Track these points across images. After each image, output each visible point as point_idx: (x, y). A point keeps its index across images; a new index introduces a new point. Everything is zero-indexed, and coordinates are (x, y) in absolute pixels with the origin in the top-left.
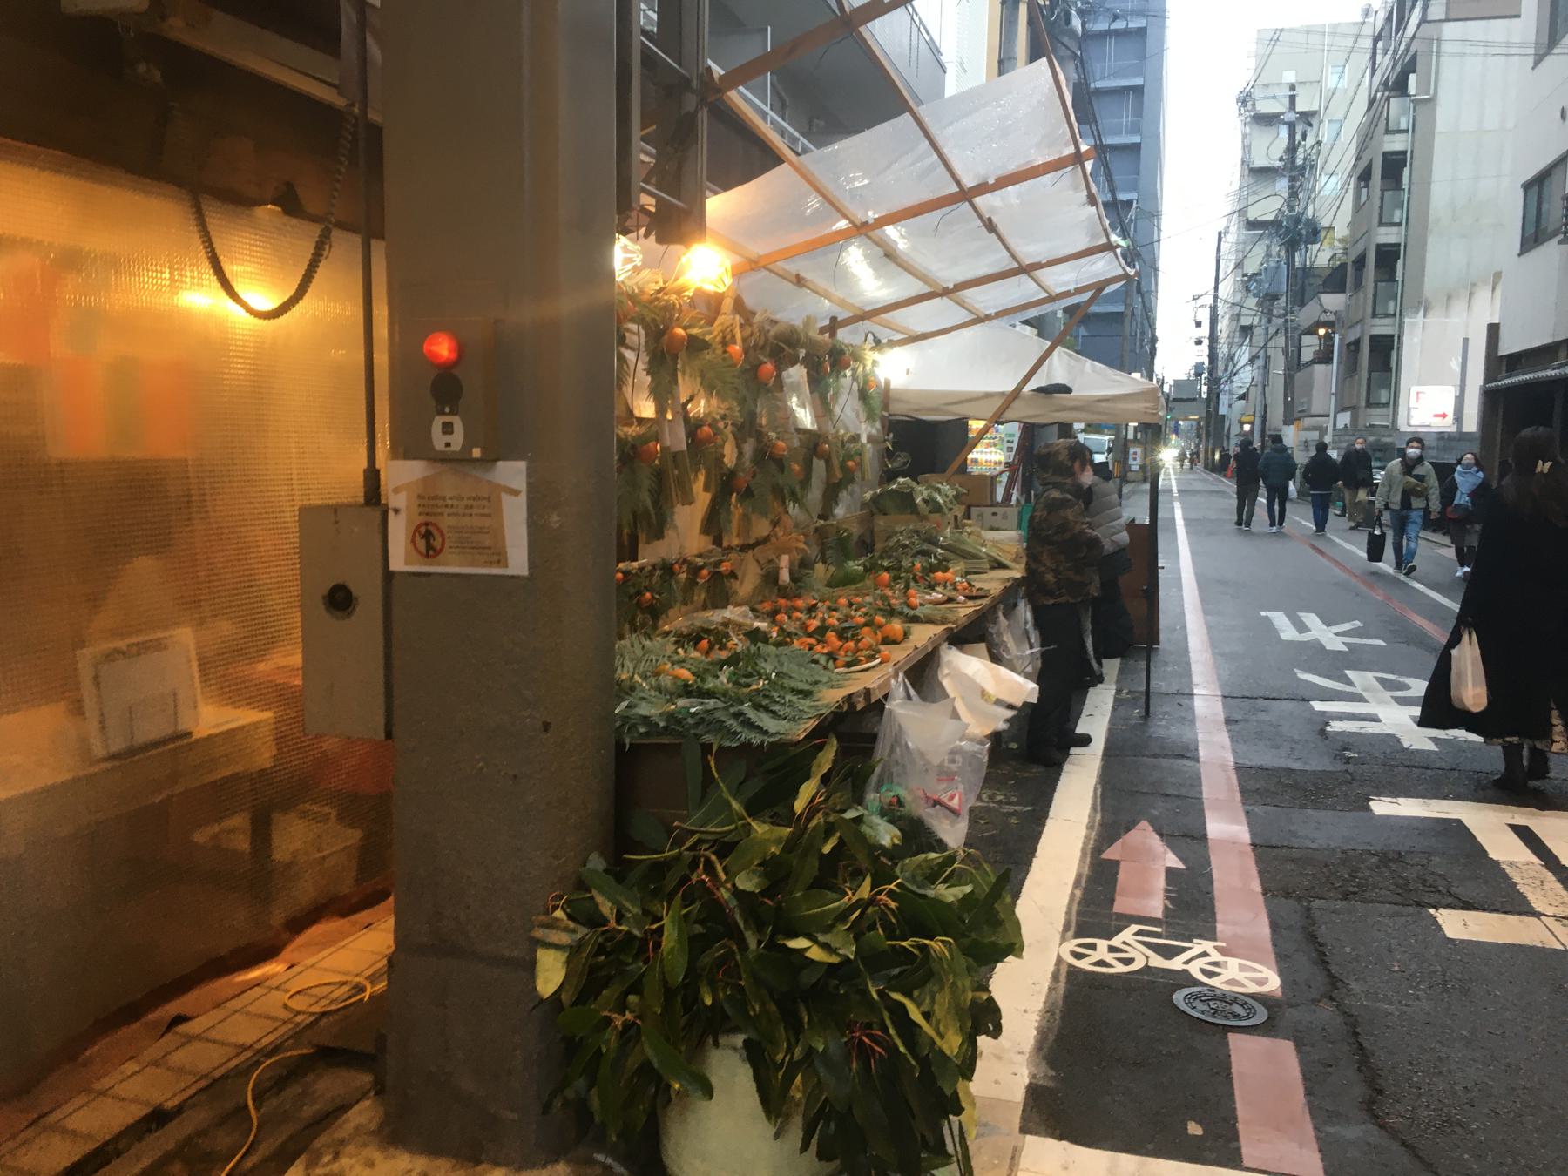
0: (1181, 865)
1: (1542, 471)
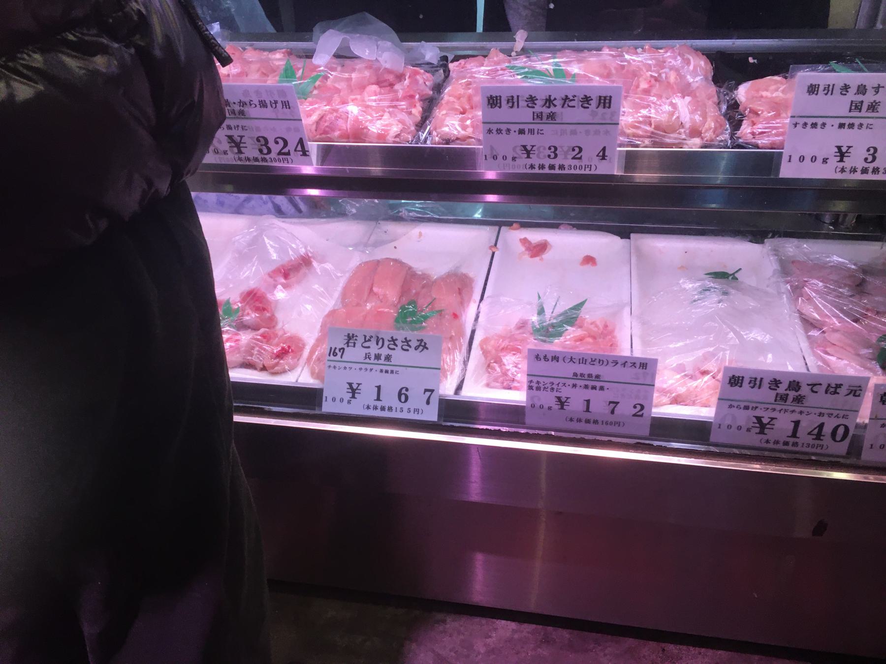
0: (313, 287)
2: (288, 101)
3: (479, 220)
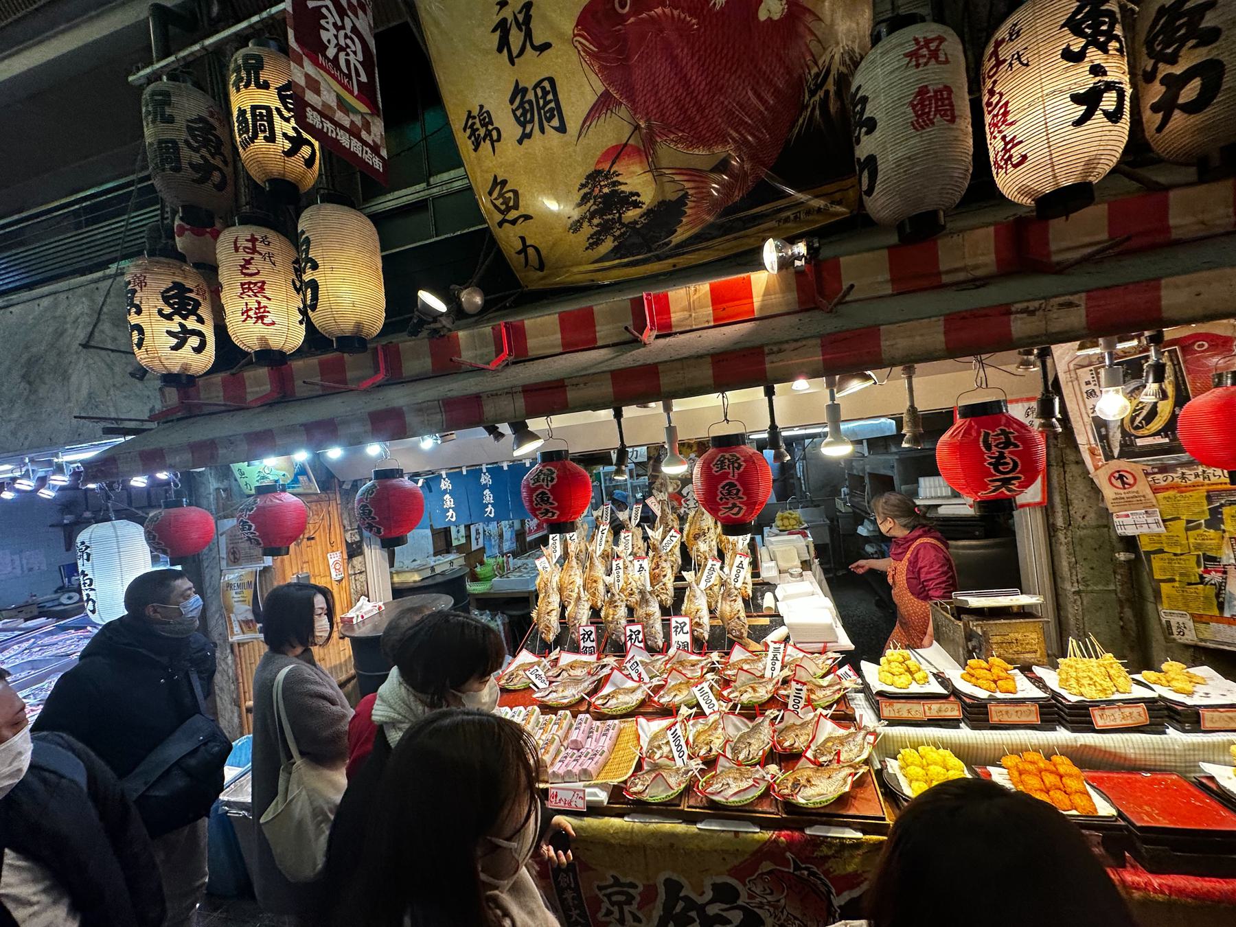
0: (853, 647)
1: (770, 19)
2: (551, 81)
3: (826, 571)
